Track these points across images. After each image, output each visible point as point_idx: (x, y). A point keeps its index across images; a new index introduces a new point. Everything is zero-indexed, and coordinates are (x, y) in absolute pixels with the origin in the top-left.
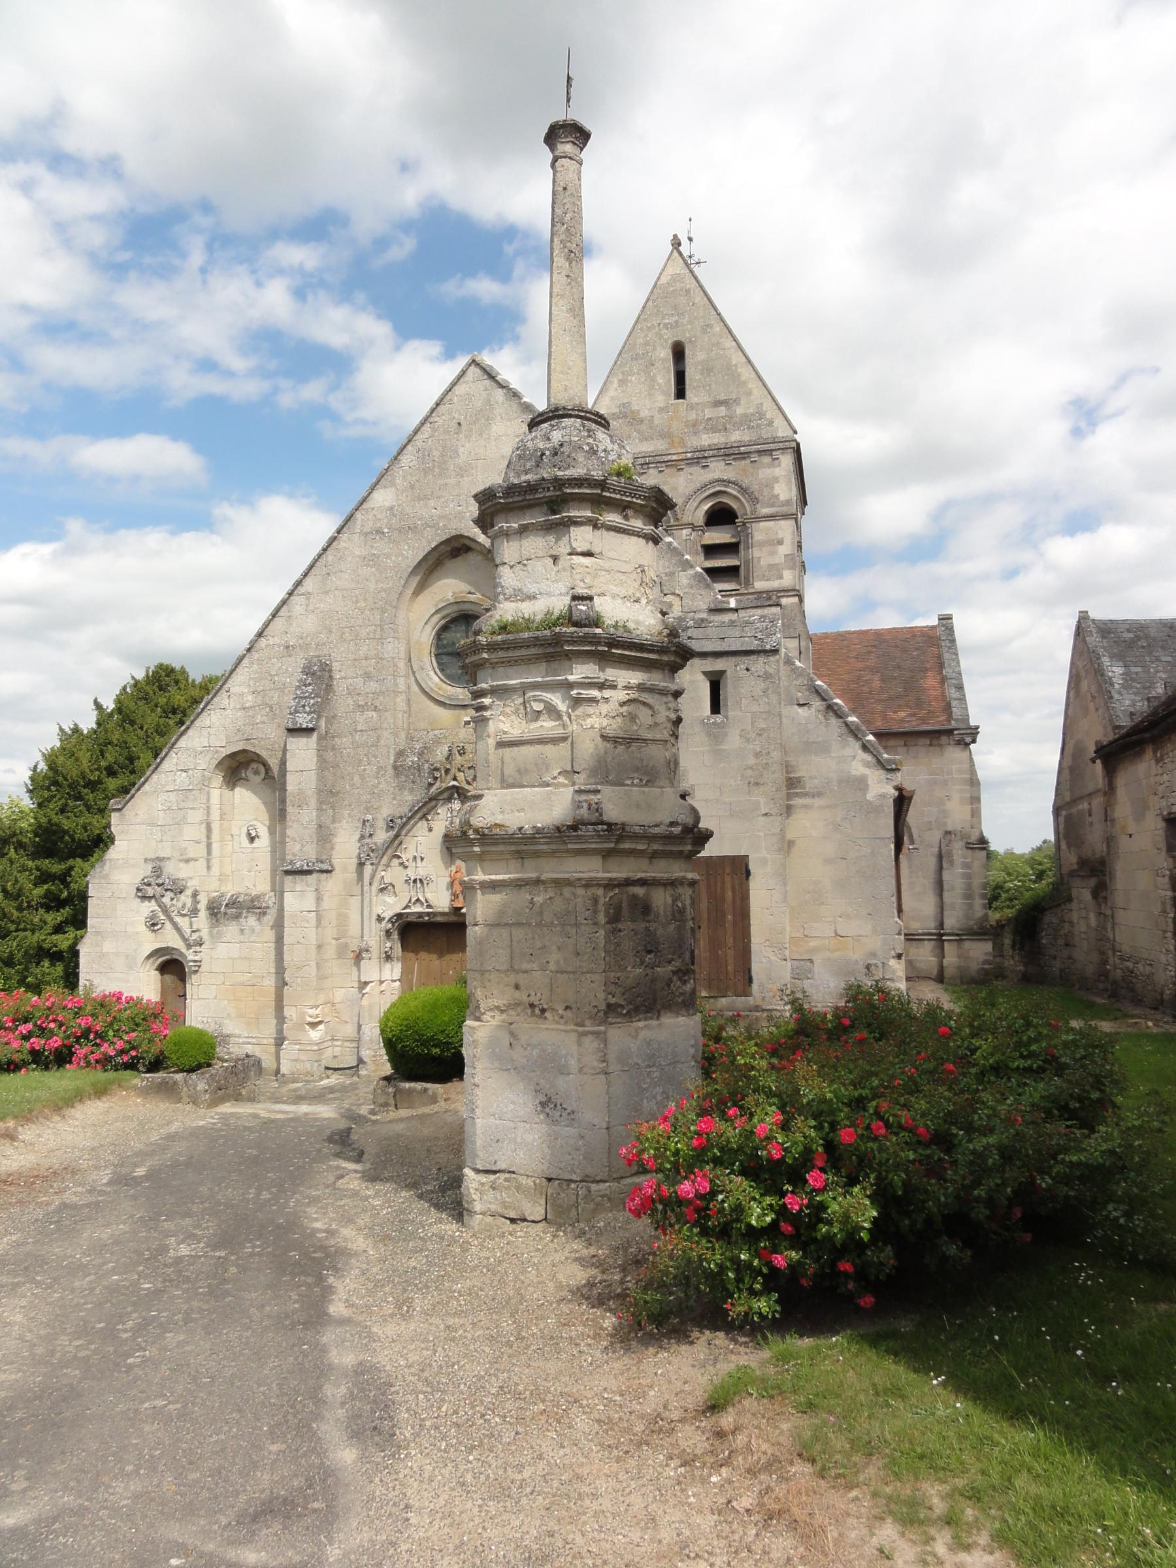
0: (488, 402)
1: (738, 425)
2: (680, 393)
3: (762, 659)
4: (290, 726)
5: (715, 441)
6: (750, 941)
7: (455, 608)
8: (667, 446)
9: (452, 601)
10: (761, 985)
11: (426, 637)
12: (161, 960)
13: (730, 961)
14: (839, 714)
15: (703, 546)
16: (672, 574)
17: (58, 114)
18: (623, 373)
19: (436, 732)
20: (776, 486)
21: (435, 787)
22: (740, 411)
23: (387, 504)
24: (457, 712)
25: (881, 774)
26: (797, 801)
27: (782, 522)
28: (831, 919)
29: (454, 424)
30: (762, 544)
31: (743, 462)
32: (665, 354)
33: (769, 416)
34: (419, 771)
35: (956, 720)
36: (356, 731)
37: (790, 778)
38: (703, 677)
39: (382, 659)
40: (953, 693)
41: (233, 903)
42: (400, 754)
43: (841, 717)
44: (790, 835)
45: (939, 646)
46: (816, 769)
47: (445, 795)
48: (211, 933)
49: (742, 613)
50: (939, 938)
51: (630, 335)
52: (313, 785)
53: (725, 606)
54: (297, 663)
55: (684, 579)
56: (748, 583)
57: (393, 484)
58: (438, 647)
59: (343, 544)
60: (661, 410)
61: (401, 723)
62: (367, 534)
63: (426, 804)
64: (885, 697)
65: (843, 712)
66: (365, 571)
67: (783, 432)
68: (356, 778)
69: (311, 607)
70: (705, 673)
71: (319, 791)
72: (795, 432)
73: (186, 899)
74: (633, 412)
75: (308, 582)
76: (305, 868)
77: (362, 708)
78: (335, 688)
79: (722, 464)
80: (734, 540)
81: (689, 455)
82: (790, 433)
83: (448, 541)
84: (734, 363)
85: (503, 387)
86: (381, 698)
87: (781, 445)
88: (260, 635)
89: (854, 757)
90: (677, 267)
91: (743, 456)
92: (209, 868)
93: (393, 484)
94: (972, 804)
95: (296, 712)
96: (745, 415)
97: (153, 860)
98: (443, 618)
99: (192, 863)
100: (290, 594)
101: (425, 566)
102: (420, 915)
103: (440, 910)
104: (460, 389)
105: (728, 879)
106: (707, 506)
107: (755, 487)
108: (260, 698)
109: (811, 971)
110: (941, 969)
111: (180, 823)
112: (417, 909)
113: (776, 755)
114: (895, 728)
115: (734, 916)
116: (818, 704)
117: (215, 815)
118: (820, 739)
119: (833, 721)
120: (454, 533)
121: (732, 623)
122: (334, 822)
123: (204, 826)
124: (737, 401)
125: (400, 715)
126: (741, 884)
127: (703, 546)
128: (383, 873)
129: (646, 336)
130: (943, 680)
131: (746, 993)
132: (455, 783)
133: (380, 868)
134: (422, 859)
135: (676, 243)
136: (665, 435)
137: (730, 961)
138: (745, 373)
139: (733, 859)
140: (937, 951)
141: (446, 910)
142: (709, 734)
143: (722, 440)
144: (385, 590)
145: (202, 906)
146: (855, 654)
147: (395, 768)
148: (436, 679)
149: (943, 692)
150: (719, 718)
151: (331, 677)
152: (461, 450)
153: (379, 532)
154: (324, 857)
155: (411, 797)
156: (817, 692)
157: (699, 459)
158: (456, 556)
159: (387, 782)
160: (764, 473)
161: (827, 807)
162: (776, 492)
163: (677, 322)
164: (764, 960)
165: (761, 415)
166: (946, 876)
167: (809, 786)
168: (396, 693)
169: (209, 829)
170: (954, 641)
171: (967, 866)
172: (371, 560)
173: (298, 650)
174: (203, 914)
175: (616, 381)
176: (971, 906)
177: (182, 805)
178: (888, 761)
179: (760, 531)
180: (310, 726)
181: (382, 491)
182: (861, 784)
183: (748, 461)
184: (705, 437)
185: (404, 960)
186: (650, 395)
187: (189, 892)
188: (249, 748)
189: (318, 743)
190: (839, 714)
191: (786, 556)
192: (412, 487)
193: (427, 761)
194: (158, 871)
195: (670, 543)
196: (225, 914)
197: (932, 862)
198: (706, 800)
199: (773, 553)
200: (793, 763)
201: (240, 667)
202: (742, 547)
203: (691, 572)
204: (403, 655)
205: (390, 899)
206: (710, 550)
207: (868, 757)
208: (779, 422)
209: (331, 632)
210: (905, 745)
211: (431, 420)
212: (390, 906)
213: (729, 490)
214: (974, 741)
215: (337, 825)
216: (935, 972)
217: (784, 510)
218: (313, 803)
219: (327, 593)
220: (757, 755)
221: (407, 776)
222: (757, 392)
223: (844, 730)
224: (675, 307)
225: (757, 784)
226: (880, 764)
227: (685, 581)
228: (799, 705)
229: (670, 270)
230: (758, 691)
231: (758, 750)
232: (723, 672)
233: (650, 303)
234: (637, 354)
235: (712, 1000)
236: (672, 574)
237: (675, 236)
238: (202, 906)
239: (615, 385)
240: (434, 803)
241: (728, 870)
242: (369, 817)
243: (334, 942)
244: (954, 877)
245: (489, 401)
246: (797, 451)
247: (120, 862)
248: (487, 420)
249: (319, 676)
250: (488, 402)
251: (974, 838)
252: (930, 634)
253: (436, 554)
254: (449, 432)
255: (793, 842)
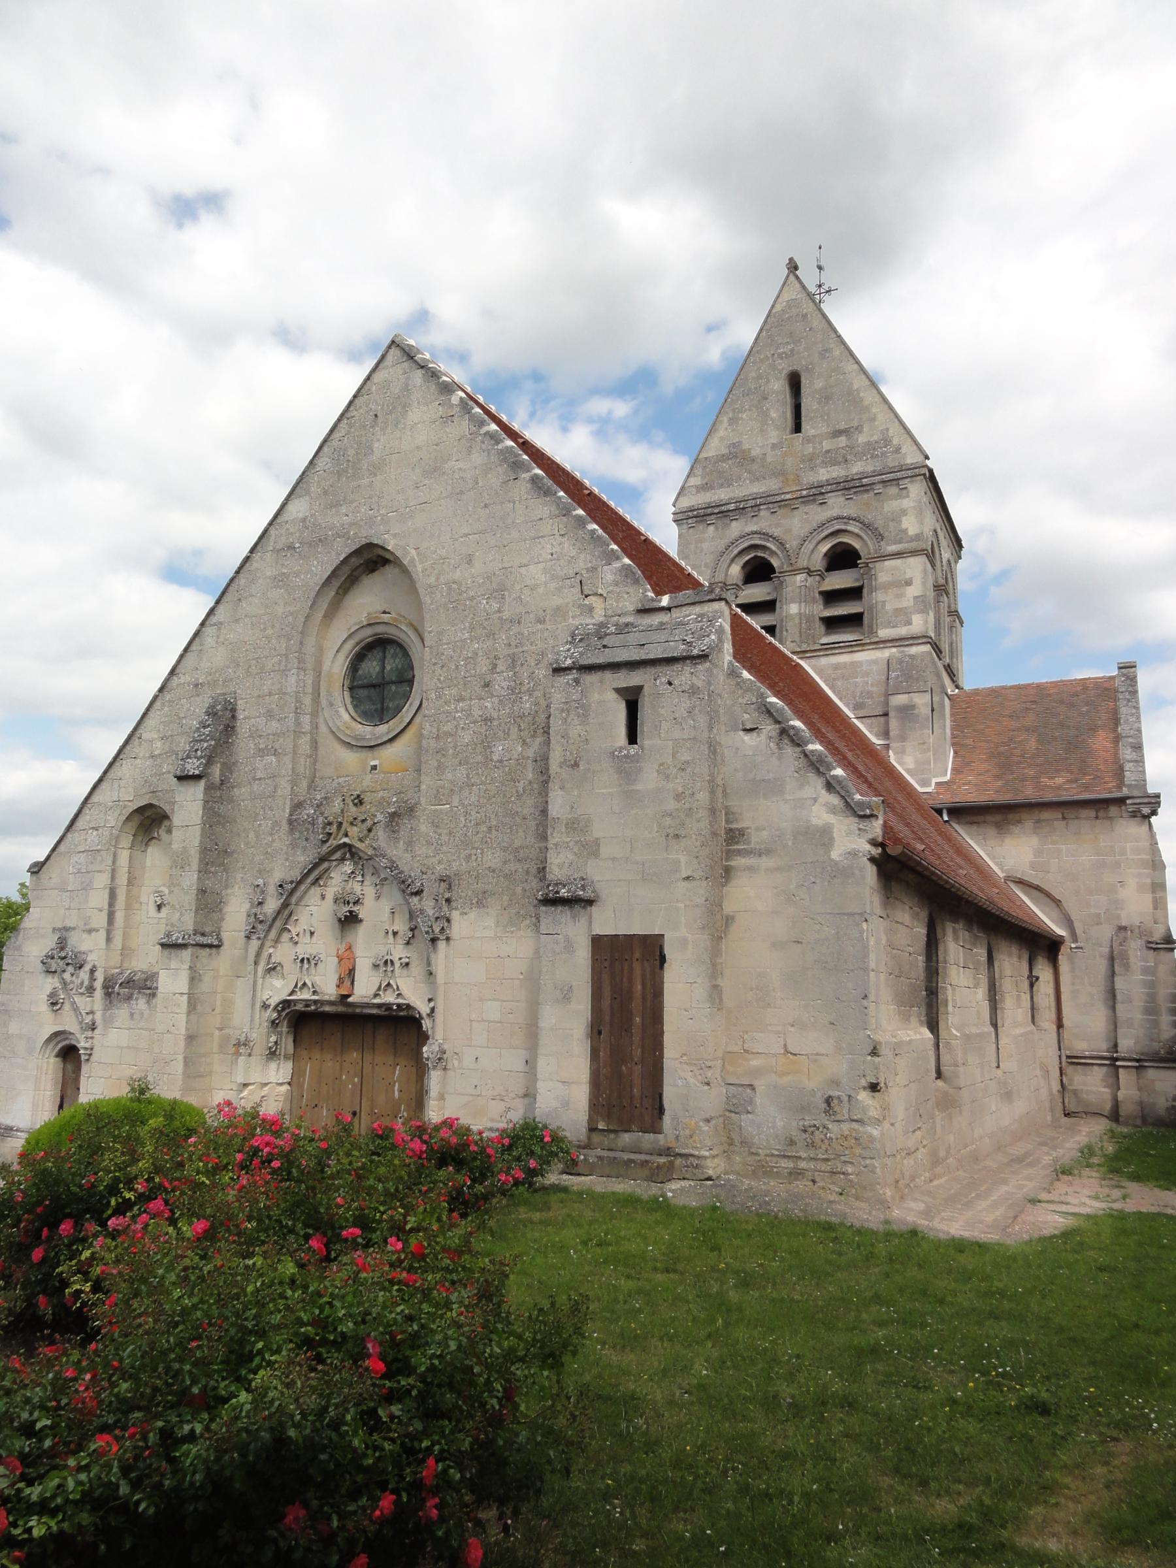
0: (406, 388)
1: (859, 456)
2: (797, 428)
3: (688, 668)
4: (178, 773)
5: (834, 475)
6: (661, 1056)
7: (369, 632)
8: (781, 485)
9: (365, 623)
10: (674, 1118)
11: (337, 666)
12: (60, 1046)
13: (637, 1081)
14: (797, 741)
15: (821, 593)
16: (593, 570)
17: (422, 318)
18: (734, 411)
19: (341, 780)
20: (904, 519)
21: (328, 844)
22: (862, 439)
23: (301, 515)
24: (364, 754)
25: (852, 821)
26: (739, 862)
27: (911, 560)
28: (780, 1028)
29: (371, 417)
30: (887, 587)
31: (866, 496)
32: (779, 385)
33: (895, 442)
34: (313, 824)
35: (1129, 786)
36: (255, 780)
37: (731, 830)
38: (614, 696)
39: (285, 694)
40: (1127, 754)
41: (128, 983)
42: (297, 806)
43: (799, 745)
44: (728, 908)
45: (1116, 700)
46: (764, 817)
47: (338, 855)
48: (104, 1015)
49: (676, 613)
50: (1113, 1062)
51: (741, 369)
52: (197, 842)
53: (656, 605)
54: (203, 702)
55: (609, 573)
56: (872, 632)
57: (308, 493)
58: (353, 679)
59: (255, 565)
60: (774, 446)
61: (302, 769)
62: (279, 551)
63: (316, 866)
64: (1039, 761)
65: (801, 738)
66: (276, 594)
67: (912, 458)
68: (252, 835)
69: (221, 639)
70: (617, 690)
71: (204, 851)
72: (927, 458)
73: (84, 975)
74: (744, 451)
75: (221, 609)
76: (180, 941)
77: (262, 753)
78: (238, 729)
79: (842, 499)
80: (857, 584)
81: (804, 493)
82: (920, 458)
83: (357, 552)
84: (856, 387)
85: (422, 367)
86: (281, 740)
87: (909, 473)
88: (173, 672)
89: (815, 800)
90: (793, 292)
91: (865, 488)
92: (109, 940)
93: (308, 493)
94: (1153, 892)
95: (188, 757)
96: (868, 443)
97: (60, 930)
98: (358, 644)
99: (94, 934)
100: (202, 624)
101: (336, 583)
102: (307, 1003)
103: (327, 998)
104: (378, 377)
105: (637, 966)
106: (825, 547)
107: (879, 523)
108: (168, 744)
109: (751, 1101)
110: (1116, 1104)
111: (87, 888)
112: (306, 995)
113: (703, 796)
114: (1050, 797)
115: (643, 1019)
116: (769, 728)
117: (122, 879)
118: (771, 776)
119: (790, 751)
120: (364, 541)
121: (661, 627)
122: (226, 887)
123: (107, 891)
124: (859, 429)
125: (302, 760)
126: (653, 974)
127: (821, 593)
128: (271, 950)
129: (759, 368)
130: (1117, 739)
131: (655, 1129)
132: (346, 840)
133: (268, 943)
134: (312, 933)
135: (793, 267)
136: (780, 473)
137: (637, 1081)
138: (869, 397)
139: (645, 938)
140: (1111, 1080)
141: (332, 998)
142: (620, 771)
143: (843, 473)
144: (292, 614)
145: (98, 984)
146: (1007, 712)
147: (290, 822)
148: (346, 717)
149: (1116, 754)
150: (633, 750)
151: (234, 717)
152: (376, 445)
153: (291, 547)
154: (207, 930)
155: (304, 858)
156: (768, 711)
157: (816, 495)
158: (373, 571)
159: (281, 840)
160: (891, 506)
161: (778, 869)
162: (904, 526)
163: (792, 350)
164: (680, 1082)
165: (887, 441)
166: (1119, 983)
167: (756, 839)
168: (298, 733)
169: (113, 895)
170: (1136, 692)
171: (1146, 971)
172: (280, 580)
173: (206, 688)
174: (99, 993)
175: (725, 419)
176: (1156, 1024)
177: (91, 867)
178: (861, 804)
179: (885, 572)
180: (197, 772)
181: (296, 501)
182: (824, 837)
183: (871, 494)
184: (822, 471)
185: (295, 1057)
186: (762, 431)
187: (87, 968)
188: (155, 802)
189: (205, 793)
190: (797, 741)
191: (915, 598)
192: (326, 493)
193: (322, 814)
194: (62, 944)
195: (594, 531)
196: (118, 994)
197: (1102, 966)
198: (613, 859)
199: (900, 596)
200: (735, 810)
201: (152, 711)
202: (865, 591)
203: (617, 565)
204: (309, 689)
205: (277, 983)
206: (831, 597)
207: (835, 800)
208: (907, 448)
209: (238, 665)
210: (1064, 818)
211: (348, 415)
212: (277, 990)
213: (849, 528)
214: (1154, 813)
215: (229, 891)
216: (1108, 1106)
217: (913, 545)
218: (195, 864)
219: (237, 621)
220: (678, 797)
221: (301, 833)
222: (882, 417)
223: (803, 762)
224: (791, 335)
225: (677, 836)
226: (850, 808)
227: (609, 577)
228: (745, 730)
229: (786, 297)
230: (681, 712)
231: (680, 790)
232: (639, 689)
233: (764, 333)
234: (750, 390)
235: (612, 1136)
236: (593, 570)
237: (791, 260)
238: (98, 984)
239: (725, 424)
240: (326, 865)
241: (637, 955)
242: (260, 882)
243: (217, 1033)
244: (1131, 986)
245: (407, 385)
246: (932, 479)
247: (32, 932)
248: (404, 407)
249: (223, 721)
250: (406, 388)
251: (1158, 936)
252: (1107, 685)
253: (347, 570)
254: (365, 426)
255: (733, 918)
